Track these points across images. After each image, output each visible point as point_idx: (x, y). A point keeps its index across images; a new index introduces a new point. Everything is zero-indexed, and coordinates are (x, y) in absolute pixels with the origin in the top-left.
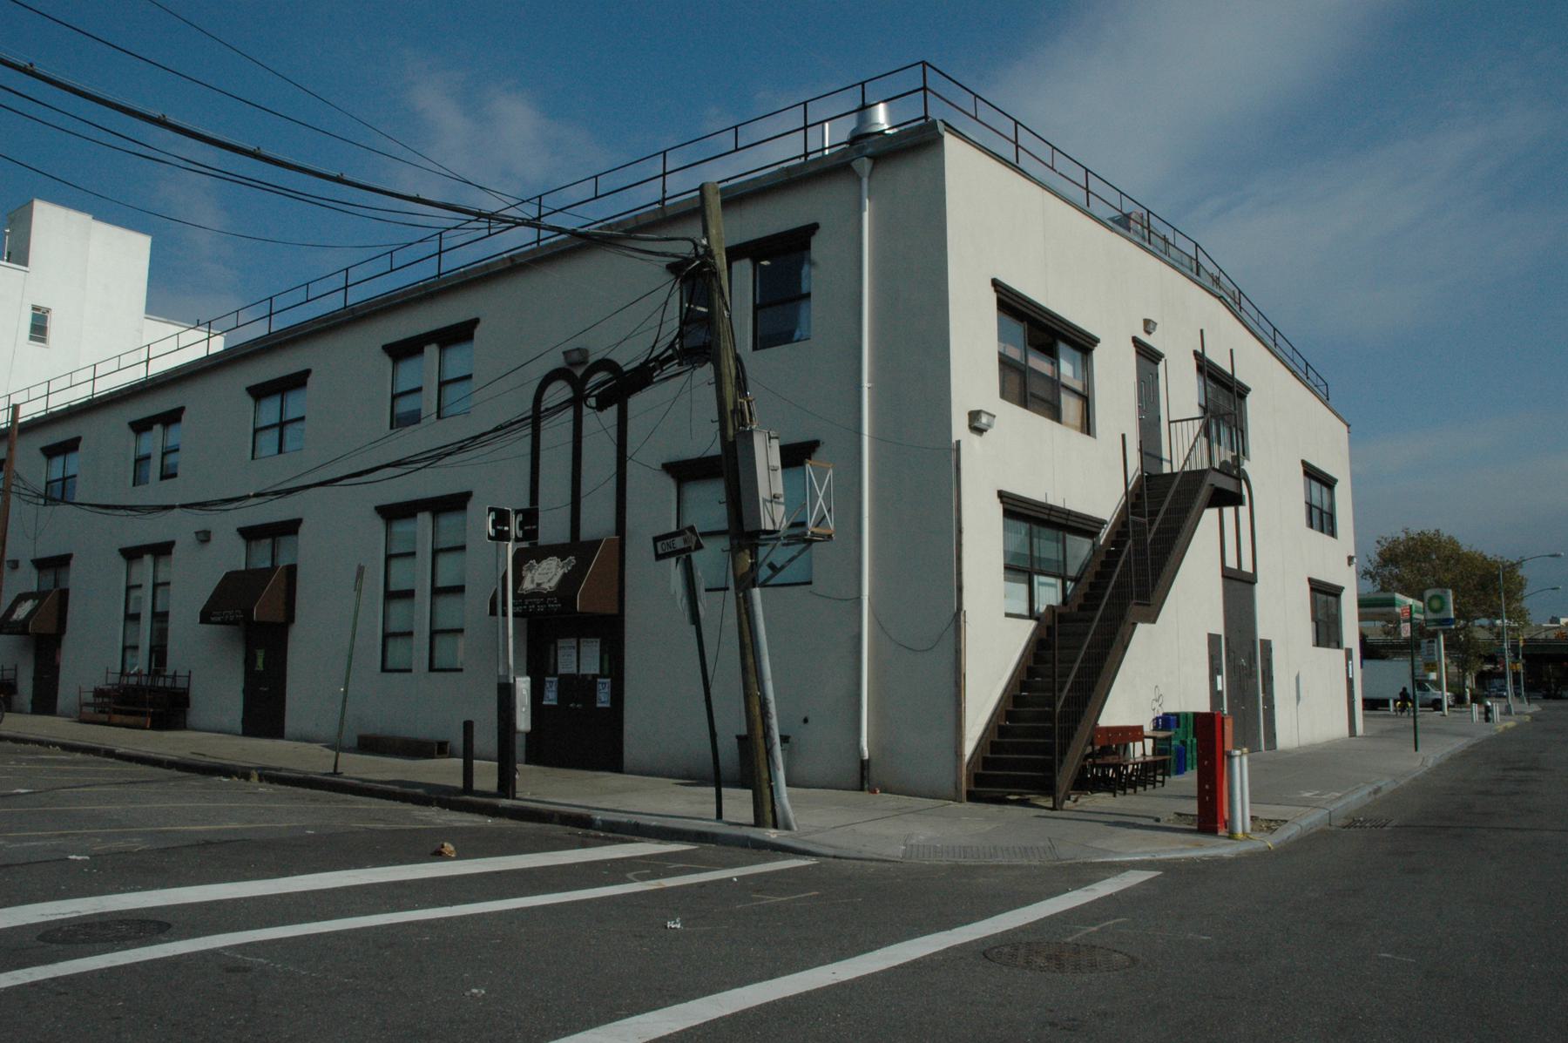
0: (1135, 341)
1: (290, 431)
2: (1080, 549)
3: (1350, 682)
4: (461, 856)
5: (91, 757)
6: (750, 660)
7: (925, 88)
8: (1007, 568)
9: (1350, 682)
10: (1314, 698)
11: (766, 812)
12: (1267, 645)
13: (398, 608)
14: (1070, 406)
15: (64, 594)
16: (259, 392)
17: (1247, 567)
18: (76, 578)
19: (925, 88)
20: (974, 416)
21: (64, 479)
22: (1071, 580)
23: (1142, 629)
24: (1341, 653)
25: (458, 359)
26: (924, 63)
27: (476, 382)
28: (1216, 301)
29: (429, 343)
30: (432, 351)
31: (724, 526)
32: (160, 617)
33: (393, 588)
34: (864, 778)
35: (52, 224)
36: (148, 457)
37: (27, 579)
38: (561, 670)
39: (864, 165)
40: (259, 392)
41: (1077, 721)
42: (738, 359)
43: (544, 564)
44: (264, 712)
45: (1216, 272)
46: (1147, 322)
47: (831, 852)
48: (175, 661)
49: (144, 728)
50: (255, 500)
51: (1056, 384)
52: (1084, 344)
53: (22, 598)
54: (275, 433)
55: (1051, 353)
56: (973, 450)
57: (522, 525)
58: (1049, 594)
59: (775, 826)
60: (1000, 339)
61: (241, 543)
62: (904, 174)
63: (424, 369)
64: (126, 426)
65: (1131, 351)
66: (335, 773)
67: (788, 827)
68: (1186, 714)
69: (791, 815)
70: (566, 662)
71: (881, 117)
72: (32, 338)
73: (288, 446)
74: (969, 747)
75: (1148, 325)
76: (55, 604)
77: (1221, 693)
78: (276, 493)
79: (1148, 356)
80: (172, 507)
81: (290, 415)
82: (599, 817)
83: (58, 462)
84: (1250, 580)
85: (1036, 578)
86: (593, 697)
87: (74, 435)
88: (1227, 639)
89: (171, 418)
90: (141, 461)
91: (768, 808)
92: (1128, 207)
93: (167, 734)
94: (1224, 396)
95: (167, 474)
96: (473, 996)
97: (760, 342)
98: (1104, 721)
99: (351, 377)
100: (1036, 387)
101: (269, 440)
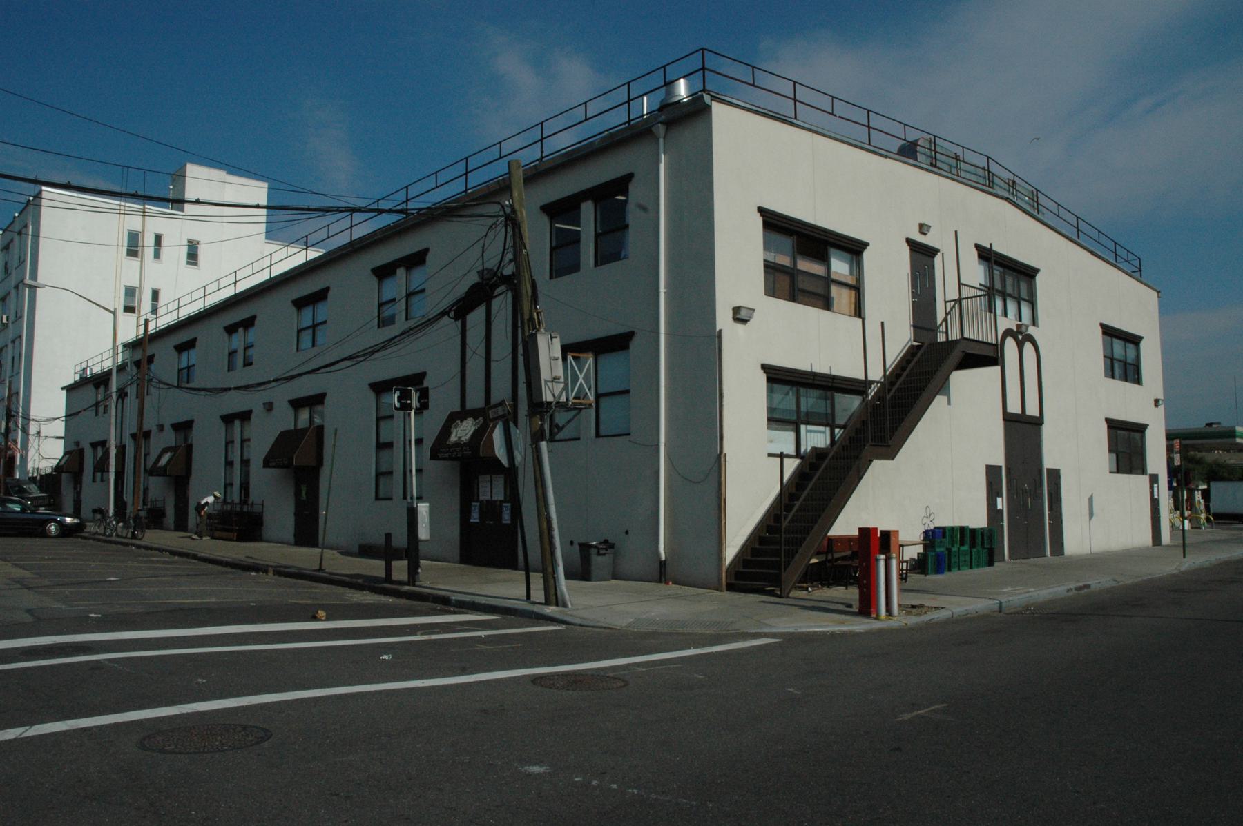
0: (909, 242)
1: (320, 332)
2: (853, 403)
3: (1155, 504)
4: (328, 619)
5: (185, 559)
6: (540, 491)
7: (703, 69)
8: (770, 420)
9: (1155, 504)
10: (1110, 518)
11: (552, 596)
12: (1055, 475)
13: (385, 454)
14: (842, 297)
15: (189, 448)
16: (300, 304)
17: (1032, 410)
18: (196, 436)
19: (703, 69)
20: (736, 310)
21: (188, 368)
22: (840, 427)
23: (878, 466)
24: (1145, 480)
25: (418, 276)
26: (703, 49)
27: (428, 292)
28: (1004, 202)
29: (400, 266)
30: (401, 272)
31: (62, 434)
32: (245, 463)
33: (382, 440)
34: (661, 573)
35: (201, 181)
36: (235, 351)
37: (169, 438)
38: (481, 498)
39: (660, 129)
40: (300, 304)
41: (807, 531)
42: (534, 285)
43: (465, 423)
44: (307, 533)
45: (1011, 176)
46: (921, 225)
47: (578, 621)
48: (254, 496)
49: (231, 540)
50: (273, 384)
51: (828, 281)
52: (854, 249)
53: (165, 451)
54: (310, 331)
55: (824, 259)
56: (732, 335)
57: (419, 399)
58: (816, 438)
59: (557, 605)
60: (765, 249)
61: (291, 411)
62: (686, 134)
63: (396, 286)
64: (222, 330)
65: (906, 250)
66: (321, 569)
67: (565, 605)
68: (952, 528)
69: (567, 597)
70: (484, 495)
71: (682, 89)
72: (188, 263)
73: (319, 340)
74: (730, 553)
75: (923, 229)
76: (184, 454)
77: (1001, 511)
78: (285, 379)
79: (922, 254)
80: (230, 389)
81: (319, 320)
82: (454, 597)
83: (184, 355)
84: (1037, 422)
85: (803, 428)
86: (499, 516)
87: (192, 337)
88: (1008, 469)
89: (248, 323)
90: (232, 354)
91: (552, 592)
92: (912, 136)
93: (244, 544)
94: (1010, 277)
95: (248, 363)
96: (198, 683)
97: (555, 272)
98: (832, 533)
99: (354, 291)
100: (803, 284)
101: (307, 337)
